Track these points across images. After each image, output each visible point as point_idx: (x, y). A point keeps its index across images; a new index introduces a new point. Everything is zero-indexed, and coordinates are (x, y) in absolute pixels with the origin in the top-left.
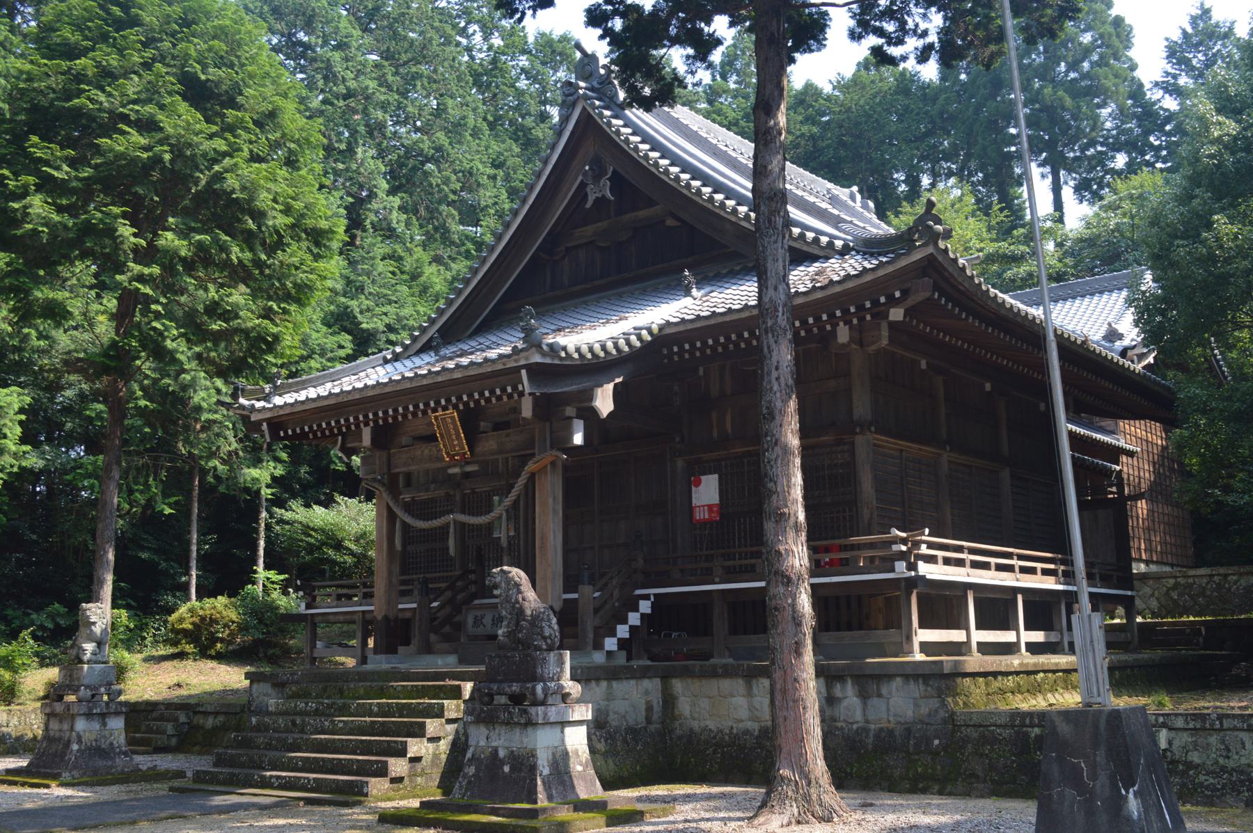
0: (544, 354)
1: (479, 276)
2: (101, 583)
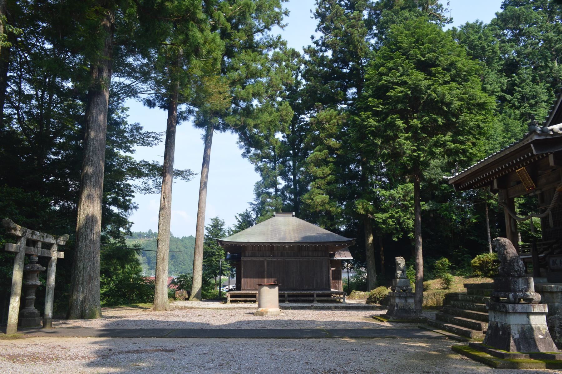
0: (539, 135)
1: (558, 104)
2: (418, 249)
